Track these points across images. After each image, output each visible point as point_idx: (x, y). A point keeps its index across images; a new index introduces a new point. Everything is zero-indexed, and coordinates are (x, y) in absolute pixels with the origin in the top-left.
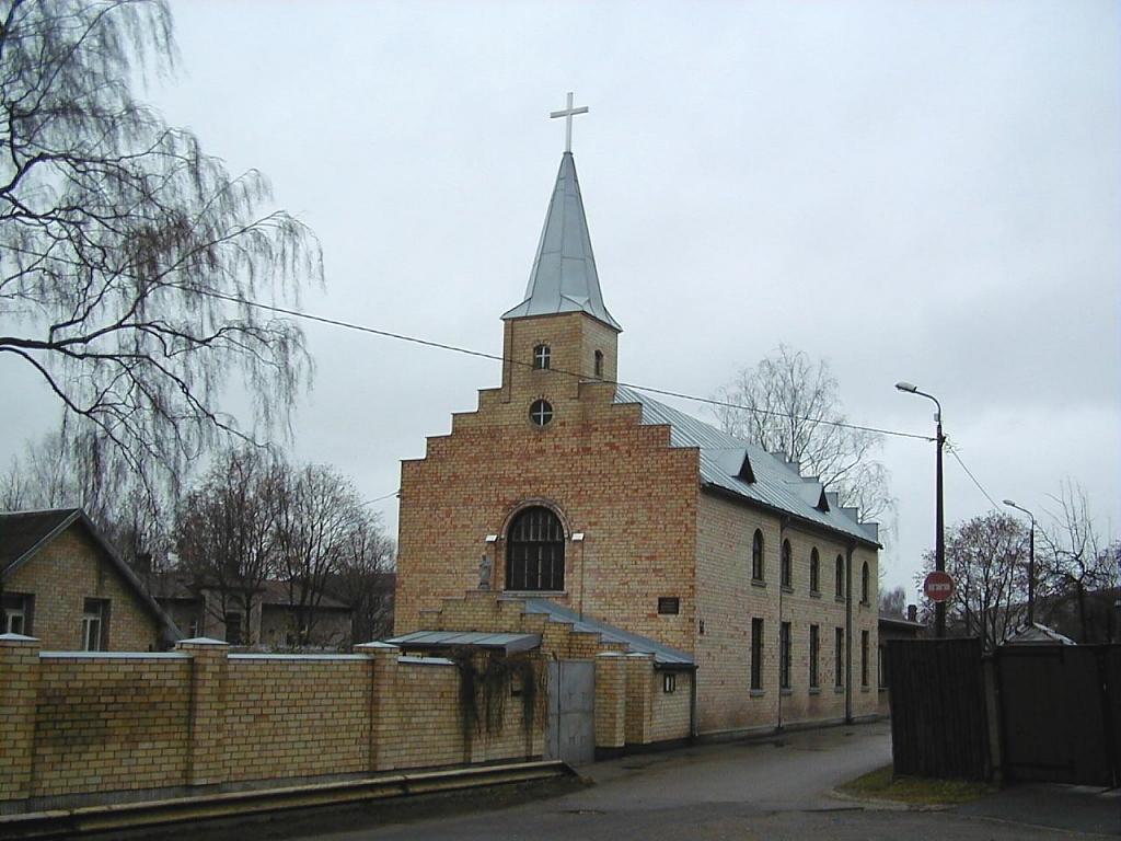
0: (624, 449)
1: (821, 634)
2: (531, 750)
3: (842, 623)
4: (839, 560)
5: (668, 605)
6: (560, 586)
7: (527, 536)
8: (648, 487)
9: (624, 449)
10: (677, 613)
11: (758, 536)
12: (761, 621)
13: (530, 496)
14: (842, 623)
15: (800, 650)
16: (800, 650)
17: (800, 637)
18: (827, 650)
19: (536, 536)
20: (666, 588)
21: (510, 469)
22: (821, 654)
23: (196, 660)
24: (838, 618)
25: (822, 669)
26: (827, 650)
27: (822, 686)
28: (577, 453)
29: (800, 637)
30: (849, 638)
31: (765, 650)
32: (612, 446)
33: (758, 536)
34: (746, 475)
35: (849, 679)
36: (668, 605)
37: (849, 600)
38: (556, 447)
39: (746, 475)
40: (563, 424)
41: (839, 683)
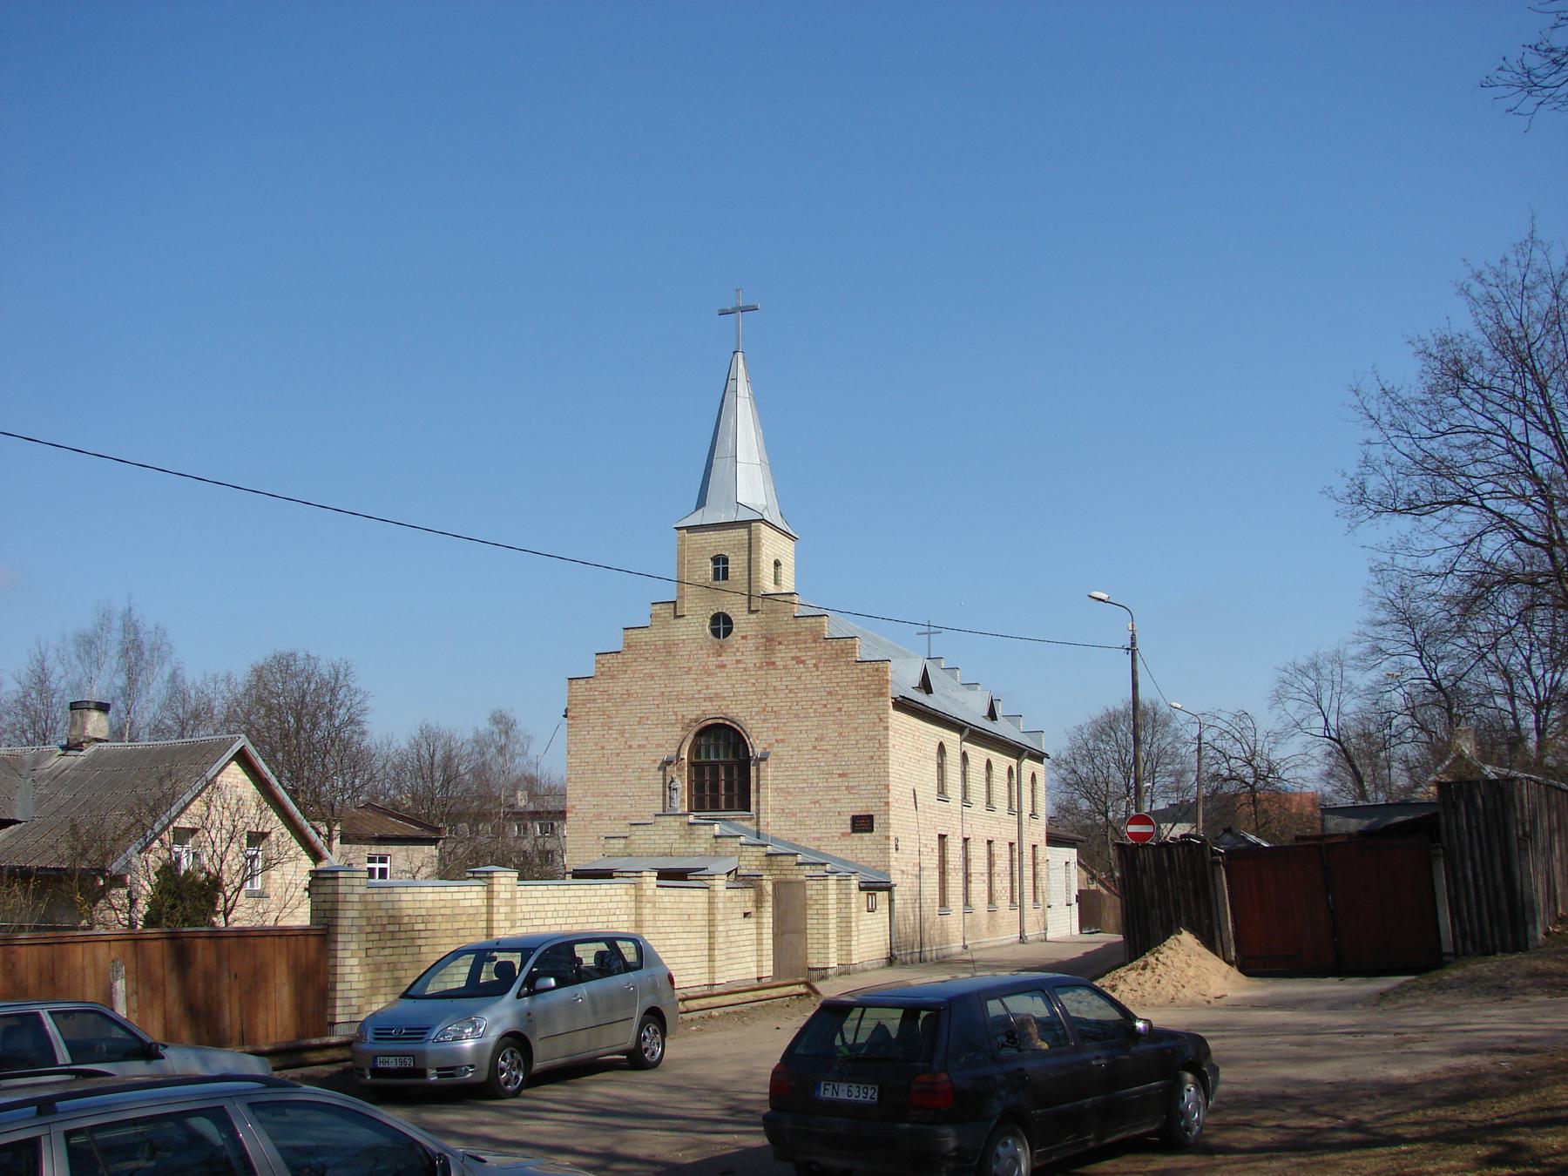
0: (810, 663)
1: (996, 848)
2: (849, 953)
3: (1014, 838)
4: (1010, 769)
5: (863, 824)
6: (746, 807)
7: (708, 755)
8: (839, 701)
9: (810, 663)
10: (872, 830)
11: (941, 748)
12: (855, 819)
13: (711, 711)
14: (1014, 838)
15: (979, 866)
16: (979, 866)
17: (978, 852)
18: (1002, 863)
19: (717, 755)
20: (860, 808)
21: (686, 685)
22: (996, 869)
23: (882, 896)
24: (1005, 830)
25: (997, 886)
26: (1002, 863)
27: (998, 903)
28: (761, 668)
29: (978, 852)
30: (1021, 853)
31: (950, 866)
32: (799, 661)
33: (941, 748)
34: (926, 685)
35: (1021, 894)
36: (863, 824)
37: (1020, 812)
38: (738, 662)
39: (926, 685)
40: (744, 638)
41: (1012, 901)
